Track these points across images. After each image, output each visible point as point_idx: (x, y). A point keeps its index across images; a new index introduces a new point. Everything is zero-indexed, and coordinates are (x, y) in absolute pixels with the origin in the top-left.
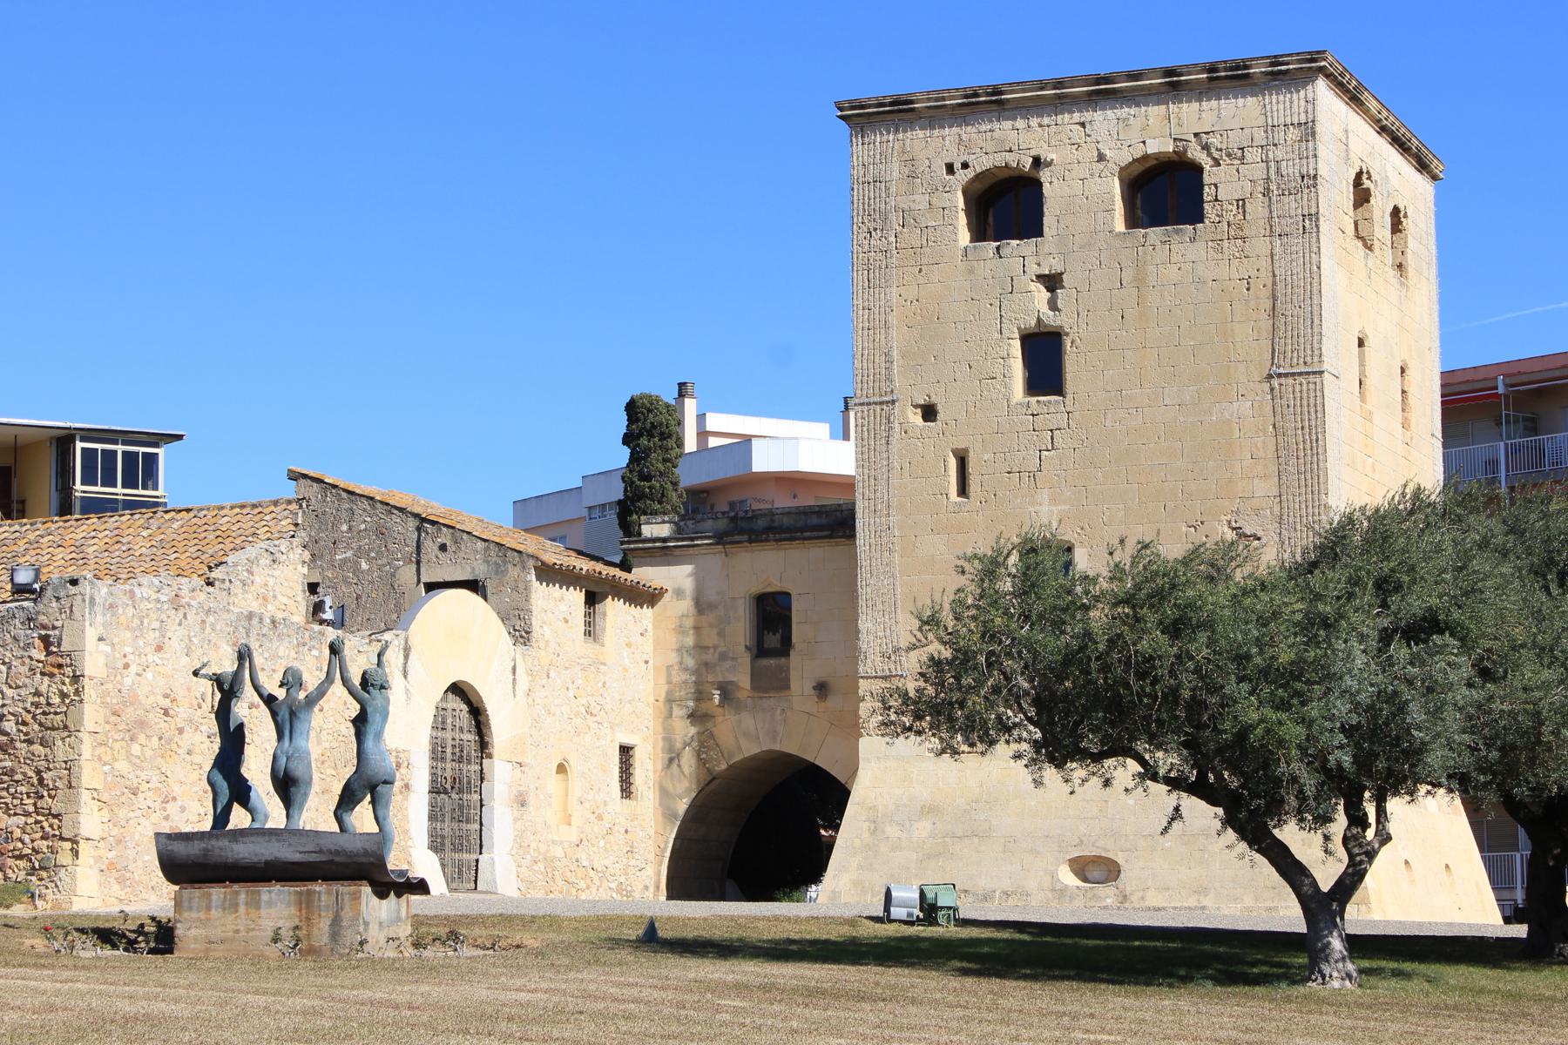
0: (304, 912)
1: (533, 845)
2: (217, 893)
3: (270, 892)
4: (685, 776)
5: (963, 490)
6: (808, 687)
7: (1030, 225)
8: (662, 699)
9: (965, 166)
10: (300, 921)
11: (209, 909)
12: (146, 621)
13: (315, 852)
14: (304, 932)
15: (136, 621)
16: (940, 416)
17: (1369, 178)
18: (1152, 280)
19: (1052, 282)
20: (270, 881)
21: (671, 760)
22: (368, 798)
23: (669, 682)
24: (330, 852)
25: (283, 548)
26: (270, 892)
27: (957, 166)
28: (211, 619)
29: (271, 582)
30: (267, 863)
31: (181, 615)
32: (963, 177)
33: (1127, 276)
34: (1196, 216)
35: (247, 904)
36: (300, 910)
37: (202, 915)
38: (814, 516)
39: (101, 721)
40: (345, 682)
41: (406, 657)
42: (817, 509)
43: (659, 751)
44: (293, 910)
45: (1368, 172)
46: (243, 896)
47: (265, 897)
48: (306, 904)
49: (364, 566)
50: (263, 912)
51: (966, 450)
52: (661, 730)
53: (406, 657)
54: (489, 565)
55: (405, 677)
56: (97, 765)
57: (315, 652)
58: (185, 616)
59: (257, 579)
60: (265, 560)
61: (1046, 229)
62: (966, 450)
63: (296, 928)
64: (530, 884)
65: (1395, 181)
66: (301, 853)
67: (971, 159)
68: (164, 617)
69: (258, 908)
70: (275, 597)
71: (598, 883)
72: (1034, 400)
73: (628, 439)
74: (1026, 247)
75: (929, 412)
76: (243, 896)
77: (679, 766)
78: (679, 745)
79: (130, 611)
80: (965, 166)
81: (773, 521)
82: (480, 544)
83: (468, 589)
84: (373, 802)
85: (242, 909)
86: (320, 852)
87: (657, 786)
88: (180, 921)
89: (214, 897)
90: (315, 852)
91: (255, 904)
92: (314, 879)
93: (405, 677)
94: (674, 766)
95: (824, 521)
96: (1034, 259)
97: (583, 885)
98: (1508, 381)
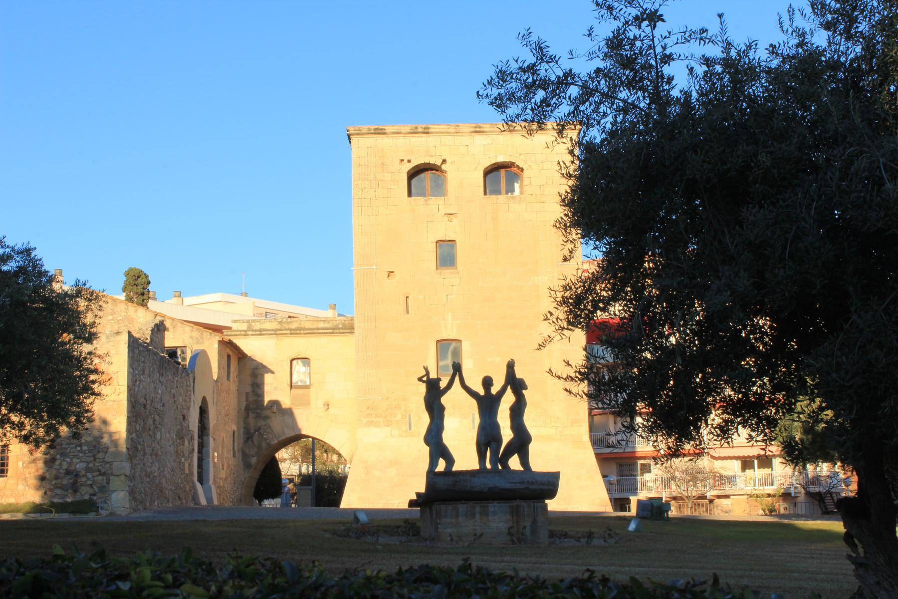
0: (515, 518)
2: (462, 507)
3: (494, 506)
4: (255, 446)
6: (320, 404)
7: (439, 189)
8: (243, 408)
9: (409, 161)
10: (513, 523)
11: (457, 516)
13: (519, 483)
14: (516, 530)
20: (488, 500)
21: (248, 439)
23: (247, 400)
24: (529, 483)
26: (494, 506)
30: (490, 489)
35: (480, 513)
36: (513, 517)
37: (453, 520)
38: (322, 322)
42: (323, 319)
43: (242, 434)
44: (508, 517)
46: (478, 509)
47: (491, 509)
48: (516, 513)
50: (490, 518)
52: (242, 423)
54: (193, 339)
63: (511, 528)
66: (511, 483)
67: (412, 159)
69: (487, 515)
74: (440, 200)
76: (478, 509)
77: (252, 441)
78: (252, 431)
81: (301, 324)
85: (478, 516)
86: (523, 483)
87: (240, 451)
88: (440, 524)
89: (460, 509)
90: (519, 483)
91: (484, 513)
92: (515, 499)
94: (250, 442)
95: (326, 325)
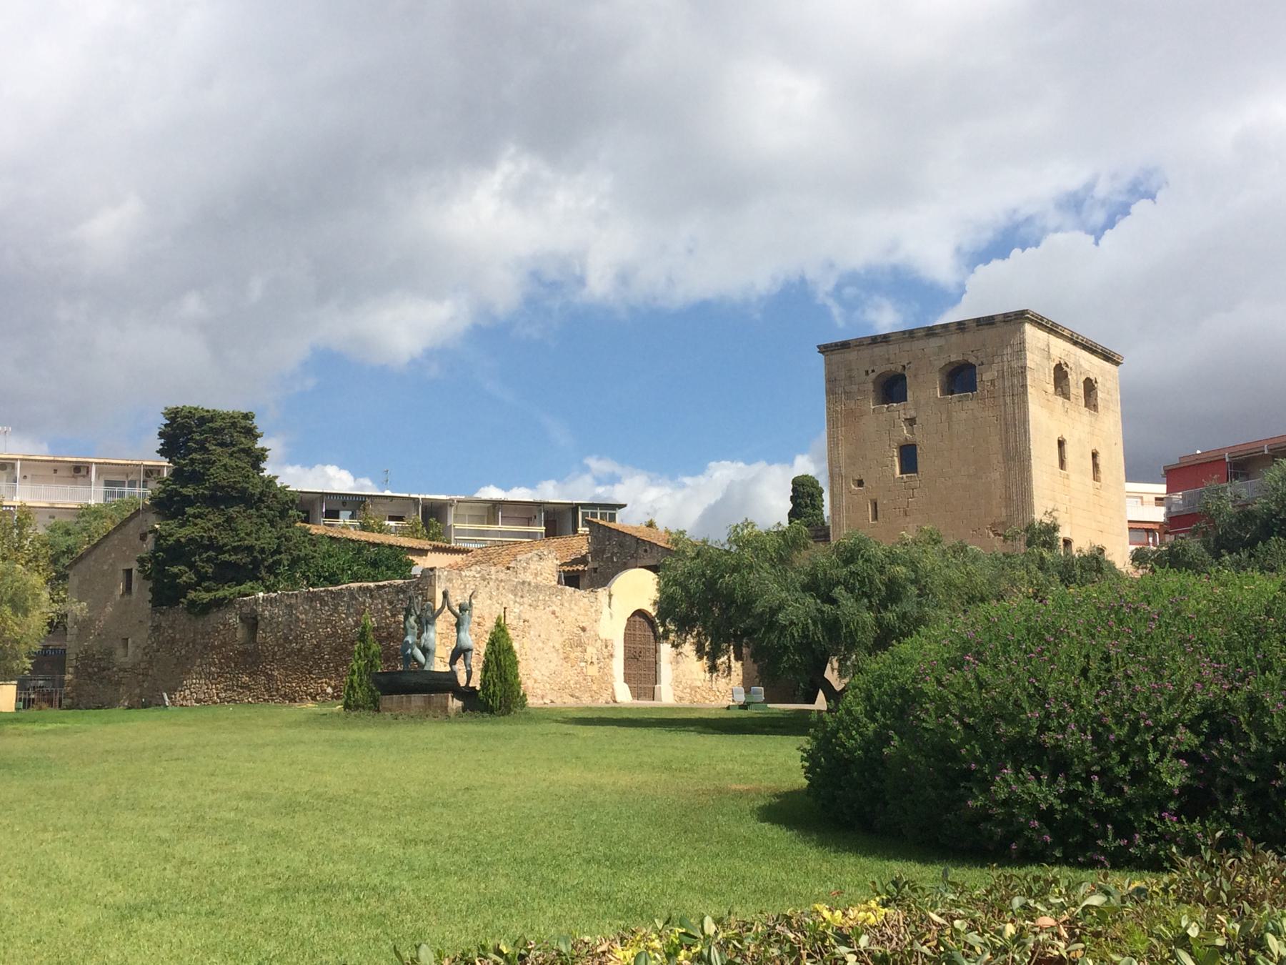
1: (684, 681)
5: (875, 517)
9: (873, 371)
12: (468, 586)
15: (462, 586)
16: (865, 484)
17: (1067, 366)
18: (954, 419)
19: (911, 422)
22: (462, 656)
25: (545, 553)
27: (870, 372)
28: (503, 584)
29: (539, 568)
31: (486, 583)
32: (873, 376)
33: (944, 418)
34: (973, 388)
39: (445, 628)
40: (450, 609)
41: (610, 598)
45: (1066, 363)
47: (413, 699)
49: (615, 560)
51: (876, 499)
53: (610, 598)
55: (610, 607)
56: (442, 646)
57: (559, 598)
58: (488, 583)
59: (532, 566)
60: (536, 558)
61: (908, 398)
62: (876, 499)
64: (681, 699)
65: (1086, 366)
67: (875, 368)
68: (477, 583)
70: (541, 574)
71: (721, 698)
72: (904, 476)
73: (792, 499)
75: (860, 483)
79: (460, 581)
80: (873, 371)
82: (660, 549)
83: (651, 570)
84: (465, 659)
93: (610, 607)
96: (903, 412)
97: (713, 699)
98: (1231, 456)
